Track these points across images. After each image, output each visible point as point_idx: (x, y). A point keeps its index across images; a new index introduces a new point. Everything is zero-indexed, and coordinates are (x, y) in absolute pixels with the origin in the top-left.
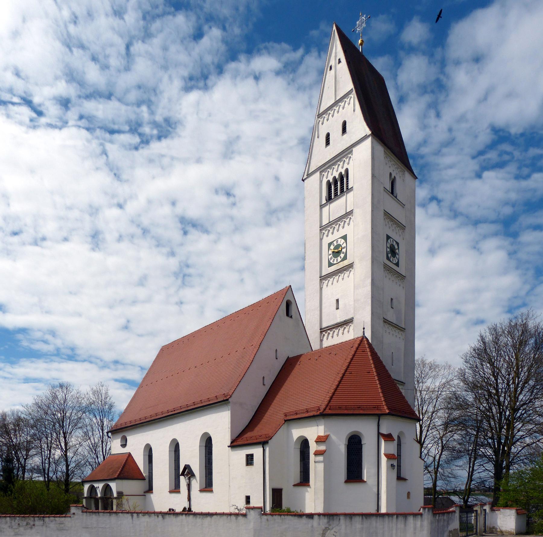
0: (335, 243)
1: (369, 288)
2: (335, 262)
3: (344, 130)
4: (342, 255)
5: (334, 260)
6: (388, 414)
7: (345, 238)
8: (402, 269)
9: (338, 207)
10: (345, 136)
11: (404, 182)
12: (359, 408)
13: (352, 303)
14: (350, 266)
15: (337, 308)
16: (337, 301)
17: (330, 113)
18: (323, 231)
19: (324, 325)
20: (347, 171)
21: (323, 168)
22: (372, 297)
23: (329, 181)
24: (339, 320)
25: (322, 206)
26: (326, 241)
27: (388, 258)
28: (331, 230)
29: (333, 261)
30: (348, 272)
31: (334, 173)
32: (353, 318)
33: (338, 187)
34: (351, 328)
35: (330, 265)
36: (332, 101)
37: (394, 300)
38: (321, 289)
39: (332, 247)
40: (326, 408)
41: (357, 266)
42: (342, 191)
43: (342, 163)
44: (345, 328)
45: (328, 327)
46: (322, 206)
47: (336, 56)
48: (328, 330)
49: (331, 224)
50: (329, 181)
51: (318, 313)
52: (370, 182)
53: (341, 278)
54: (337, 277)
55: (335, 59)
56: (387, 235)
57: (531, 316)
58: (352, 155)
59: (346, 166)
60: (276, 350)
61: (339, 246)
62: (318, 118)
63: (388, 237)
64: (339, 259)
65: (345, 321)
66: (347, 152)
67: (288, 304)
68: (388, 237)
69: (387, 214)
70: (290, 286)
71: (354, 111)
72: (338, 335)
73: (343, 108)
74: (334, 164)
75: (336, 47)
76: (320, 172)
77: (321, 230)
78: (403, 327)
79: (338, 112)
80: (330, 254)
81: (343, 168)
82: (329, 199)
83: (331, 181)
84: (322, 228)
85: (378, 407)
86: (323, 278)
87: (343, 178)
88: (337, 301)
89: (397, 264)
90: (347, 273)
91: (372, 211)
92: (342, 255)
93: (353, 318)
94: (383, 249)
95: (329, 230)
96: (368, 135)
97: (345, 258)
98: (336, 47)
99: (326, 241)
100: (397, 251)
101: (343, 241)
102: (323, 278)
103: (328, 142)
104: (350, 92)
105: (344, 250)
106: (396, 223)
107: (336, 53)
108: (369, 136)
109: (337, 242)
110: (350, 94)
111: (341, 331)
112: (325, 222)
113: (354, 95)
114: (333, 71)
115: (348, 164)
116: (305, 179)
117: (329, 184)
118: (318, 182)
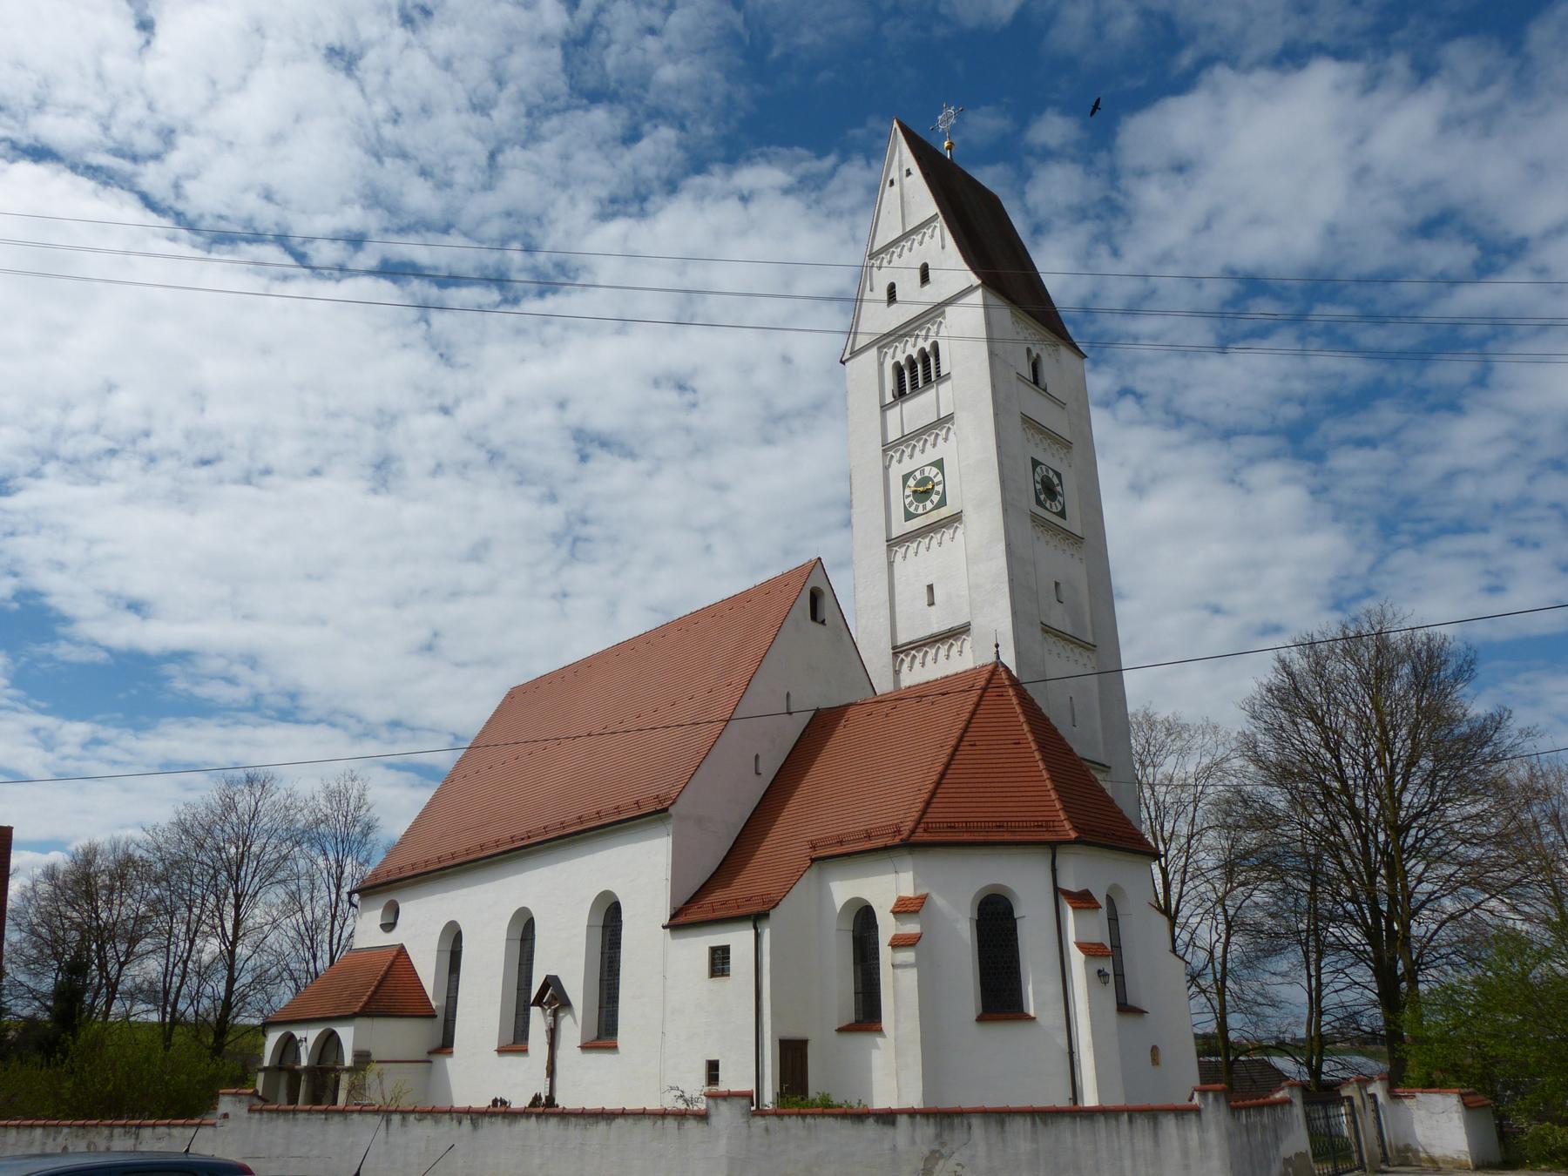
0: (917, 474)
1: (1002, 562)
7: (939, 464)
8: (1073, 523)
9: (920, 409)
10: (927, 287)
11: (1057, 364)
15: (931, 603)
20: (935, 346)
21: (884, 341)
22: (1011, 581)
24: (937, 627)
25: (884, 408)
27: (1039, 502)
31: (911, 348)
33: (919, 373)
34: (967, 645)
35: (909, 516)
36: (899, 233)
38: (891, 564)
42: (927, 379)
46: (884, 408)
47: (900, 166)
49: (905, 439)
63: (1036, 463)
67: (815, 597)
68: (1036, 463)
69: (1027, 421)
84: (887, 447)
86: (893, 543)
88: (930, 588)
90: (948, 533)
94: (1027, 485)
97: (942, 502)
101: (935, 470)
102: (893, 543)
104: (934, 218)
105: (939, 488)
106: (1050, 437)
112: (893, 435)
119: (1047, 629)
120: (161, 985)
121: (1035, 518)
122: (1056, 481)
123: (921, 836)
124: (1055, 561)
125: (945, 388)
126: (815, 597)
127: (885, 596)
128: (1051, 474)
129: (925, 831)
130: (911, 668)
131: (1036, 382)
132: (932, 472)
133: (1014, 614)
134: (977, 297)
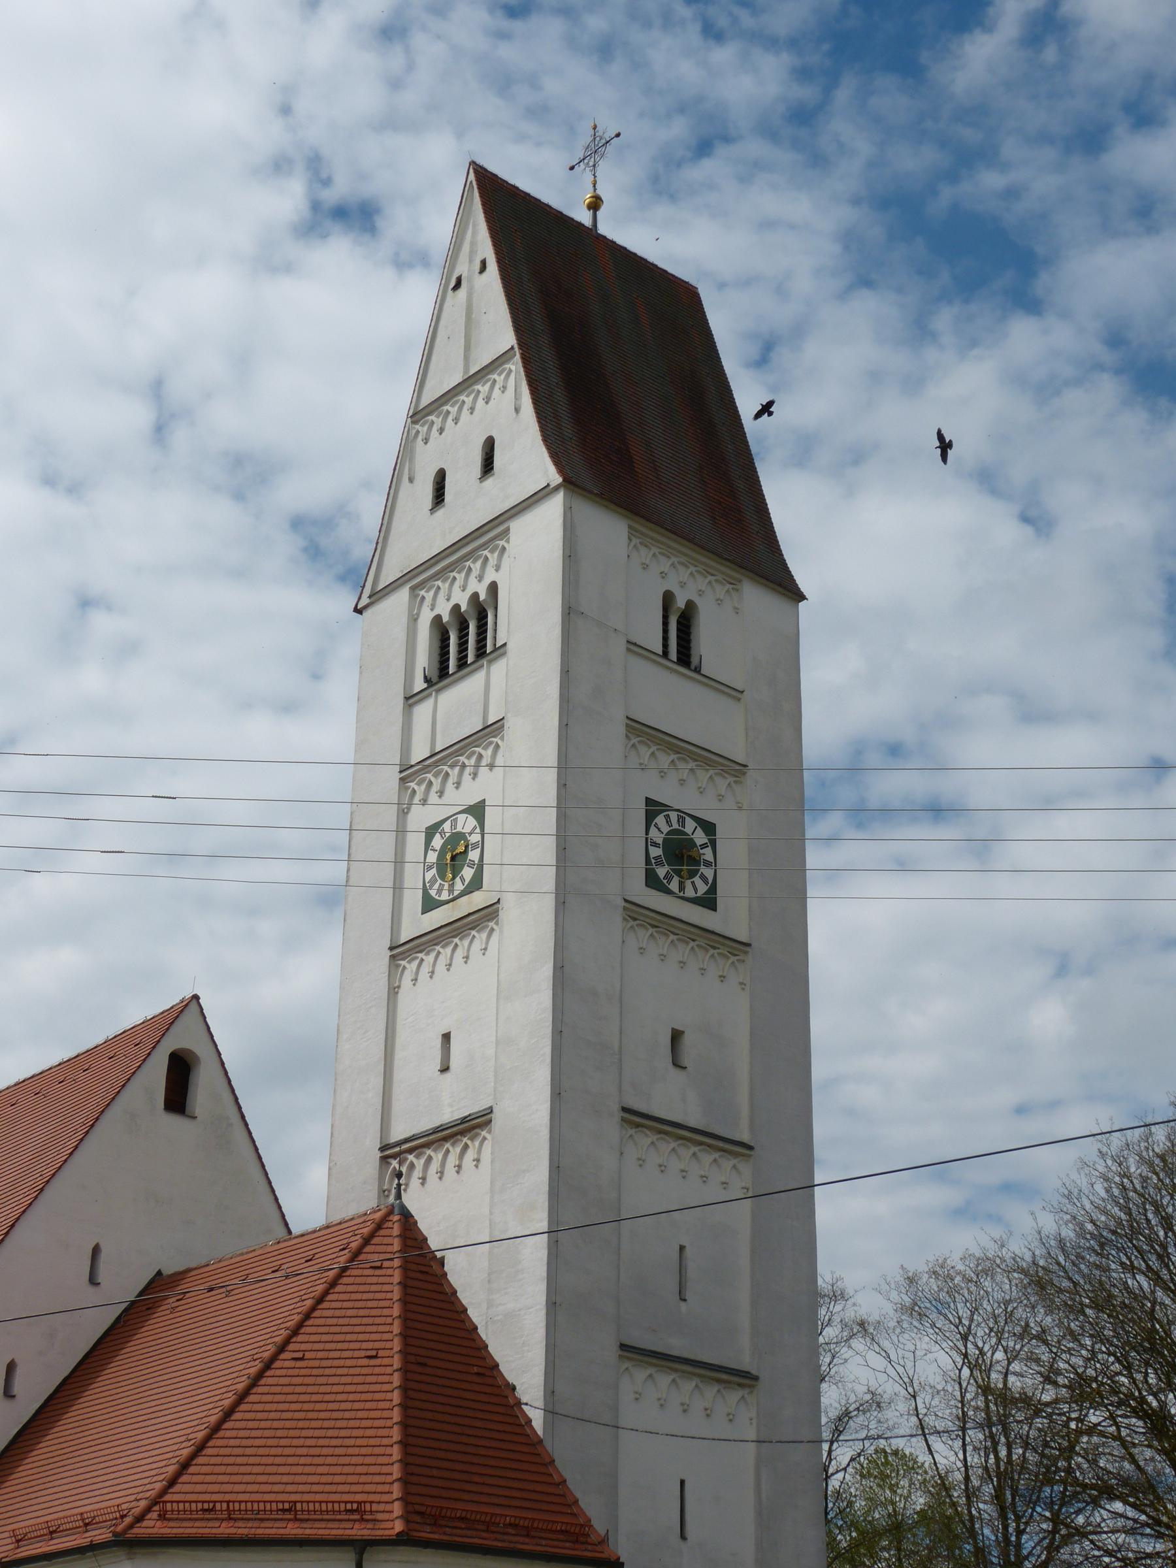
0: (447, 826)
1: (544, 998)
2: (445, 896)
3: (488, 465)
4: (468, 873)
5: (669, 822)
6: (404, 1540)
7: (477, 811)
8: (731, 917)
9: (460, 705)
10: (490, 482)
11: (729, 618)
12: (291, 1511)
13: (491, 1052)
14: (489, 914)
15: (445, 1069)
16: (447, 1037)
17: (448, 412)
18: (413, 785)
19: (399, 1132)
20: (493, 588)
21: (423, 576)
22: (558, 1033)
23: (438, 618)
24: (448, 1114)
25: (411, 700)
26: (421, 817)
27: (652, 880)
28: (421, 790)
29: (439, 891)
30: (484, 935)
31: (453, 596)
32: (490, 1110)
33: (464, 642)
34: (487, 1148)
35: (429, 904)
36: (457, 378)
37: (688, 1040)
38: (393, 991)
39: (438, 842)
40: (148, 1510)
41: (510, 912)
42: (481, 652)
43: (479, 564)
44: (466, 1147)
45: (406, 1141)
46: (411, 700)
47: (472, 253)
48: (410, 1151)
49: (438, 760)
50: (438, 618)
51: (377, 1081)
52: (557, 632)
53: (460, 953)
54: (449, 950)
55: (471, 261)
56: (649, 801)
57: (181, 1288)
58: (508, 541)
59: (490, 576)
60: (96, 1251)
61: (457, 837)
62: (414, 422)
63: (653, 809)
64: (459, 887)
65: (464, 1120)
66: (491, 533)
67: (181, 1069)
68: (653, 809)
69: (640, 731)
70: (196, 998)
71: (517, 410)
72: (441, 1174)
73: (487, 400)
74: (451, 568)
75: (474, 226)
76: (413, 589)
77: (403, 780)
78: (745, 1137)
79: (472, 410)
80: (430, 868)
81: (480, 578)
82: (441, 674)
83: (446, 618)
84: (409, 773)
85: (359, 1512)
86: (402, 951)
87: (481, 612)
88: (447, 1037)
89: (709, 902)
90: (480, 937)
91: (564, 726)
92: (468, 873)
93: (490, 1110)
94: (628, 848)
95: (430, 783)
96: (553, 485)
97: (476, 884)
98: (474, 226)
99: (421, 817)
100: (708, 854)
101: (472, 822)
102: (402, 951)
103: (439, 496)
104: (505, 357)
105: (474, 855)
106: (695, 758)
107: (473, 244)
108: (557, 488)
109: (454, 824)
110: (507, 361)
111: (452, 1160)
112: (419, 752)
113: (516, 366)
114: (462, 292)
115: (498, 568)
116: (366, 607)
117: (440, 630)
118: (404, 620)
119: (636, 1119)
120: (959, 1476)
121: (634, 912)
122: (700, 837)
123: (152, 1527)
124: (669, 987)
125: (498, 670)
126: (181, 1069)
127: (378, 1051)
128: (690, 825)
129: (162, 1517)
130: (459, 1167)
131: (685, 658)
132: (467, 824)
133: (557, 1094)
134: (556, 504)
